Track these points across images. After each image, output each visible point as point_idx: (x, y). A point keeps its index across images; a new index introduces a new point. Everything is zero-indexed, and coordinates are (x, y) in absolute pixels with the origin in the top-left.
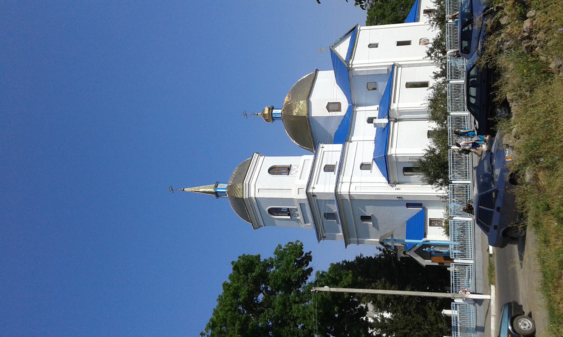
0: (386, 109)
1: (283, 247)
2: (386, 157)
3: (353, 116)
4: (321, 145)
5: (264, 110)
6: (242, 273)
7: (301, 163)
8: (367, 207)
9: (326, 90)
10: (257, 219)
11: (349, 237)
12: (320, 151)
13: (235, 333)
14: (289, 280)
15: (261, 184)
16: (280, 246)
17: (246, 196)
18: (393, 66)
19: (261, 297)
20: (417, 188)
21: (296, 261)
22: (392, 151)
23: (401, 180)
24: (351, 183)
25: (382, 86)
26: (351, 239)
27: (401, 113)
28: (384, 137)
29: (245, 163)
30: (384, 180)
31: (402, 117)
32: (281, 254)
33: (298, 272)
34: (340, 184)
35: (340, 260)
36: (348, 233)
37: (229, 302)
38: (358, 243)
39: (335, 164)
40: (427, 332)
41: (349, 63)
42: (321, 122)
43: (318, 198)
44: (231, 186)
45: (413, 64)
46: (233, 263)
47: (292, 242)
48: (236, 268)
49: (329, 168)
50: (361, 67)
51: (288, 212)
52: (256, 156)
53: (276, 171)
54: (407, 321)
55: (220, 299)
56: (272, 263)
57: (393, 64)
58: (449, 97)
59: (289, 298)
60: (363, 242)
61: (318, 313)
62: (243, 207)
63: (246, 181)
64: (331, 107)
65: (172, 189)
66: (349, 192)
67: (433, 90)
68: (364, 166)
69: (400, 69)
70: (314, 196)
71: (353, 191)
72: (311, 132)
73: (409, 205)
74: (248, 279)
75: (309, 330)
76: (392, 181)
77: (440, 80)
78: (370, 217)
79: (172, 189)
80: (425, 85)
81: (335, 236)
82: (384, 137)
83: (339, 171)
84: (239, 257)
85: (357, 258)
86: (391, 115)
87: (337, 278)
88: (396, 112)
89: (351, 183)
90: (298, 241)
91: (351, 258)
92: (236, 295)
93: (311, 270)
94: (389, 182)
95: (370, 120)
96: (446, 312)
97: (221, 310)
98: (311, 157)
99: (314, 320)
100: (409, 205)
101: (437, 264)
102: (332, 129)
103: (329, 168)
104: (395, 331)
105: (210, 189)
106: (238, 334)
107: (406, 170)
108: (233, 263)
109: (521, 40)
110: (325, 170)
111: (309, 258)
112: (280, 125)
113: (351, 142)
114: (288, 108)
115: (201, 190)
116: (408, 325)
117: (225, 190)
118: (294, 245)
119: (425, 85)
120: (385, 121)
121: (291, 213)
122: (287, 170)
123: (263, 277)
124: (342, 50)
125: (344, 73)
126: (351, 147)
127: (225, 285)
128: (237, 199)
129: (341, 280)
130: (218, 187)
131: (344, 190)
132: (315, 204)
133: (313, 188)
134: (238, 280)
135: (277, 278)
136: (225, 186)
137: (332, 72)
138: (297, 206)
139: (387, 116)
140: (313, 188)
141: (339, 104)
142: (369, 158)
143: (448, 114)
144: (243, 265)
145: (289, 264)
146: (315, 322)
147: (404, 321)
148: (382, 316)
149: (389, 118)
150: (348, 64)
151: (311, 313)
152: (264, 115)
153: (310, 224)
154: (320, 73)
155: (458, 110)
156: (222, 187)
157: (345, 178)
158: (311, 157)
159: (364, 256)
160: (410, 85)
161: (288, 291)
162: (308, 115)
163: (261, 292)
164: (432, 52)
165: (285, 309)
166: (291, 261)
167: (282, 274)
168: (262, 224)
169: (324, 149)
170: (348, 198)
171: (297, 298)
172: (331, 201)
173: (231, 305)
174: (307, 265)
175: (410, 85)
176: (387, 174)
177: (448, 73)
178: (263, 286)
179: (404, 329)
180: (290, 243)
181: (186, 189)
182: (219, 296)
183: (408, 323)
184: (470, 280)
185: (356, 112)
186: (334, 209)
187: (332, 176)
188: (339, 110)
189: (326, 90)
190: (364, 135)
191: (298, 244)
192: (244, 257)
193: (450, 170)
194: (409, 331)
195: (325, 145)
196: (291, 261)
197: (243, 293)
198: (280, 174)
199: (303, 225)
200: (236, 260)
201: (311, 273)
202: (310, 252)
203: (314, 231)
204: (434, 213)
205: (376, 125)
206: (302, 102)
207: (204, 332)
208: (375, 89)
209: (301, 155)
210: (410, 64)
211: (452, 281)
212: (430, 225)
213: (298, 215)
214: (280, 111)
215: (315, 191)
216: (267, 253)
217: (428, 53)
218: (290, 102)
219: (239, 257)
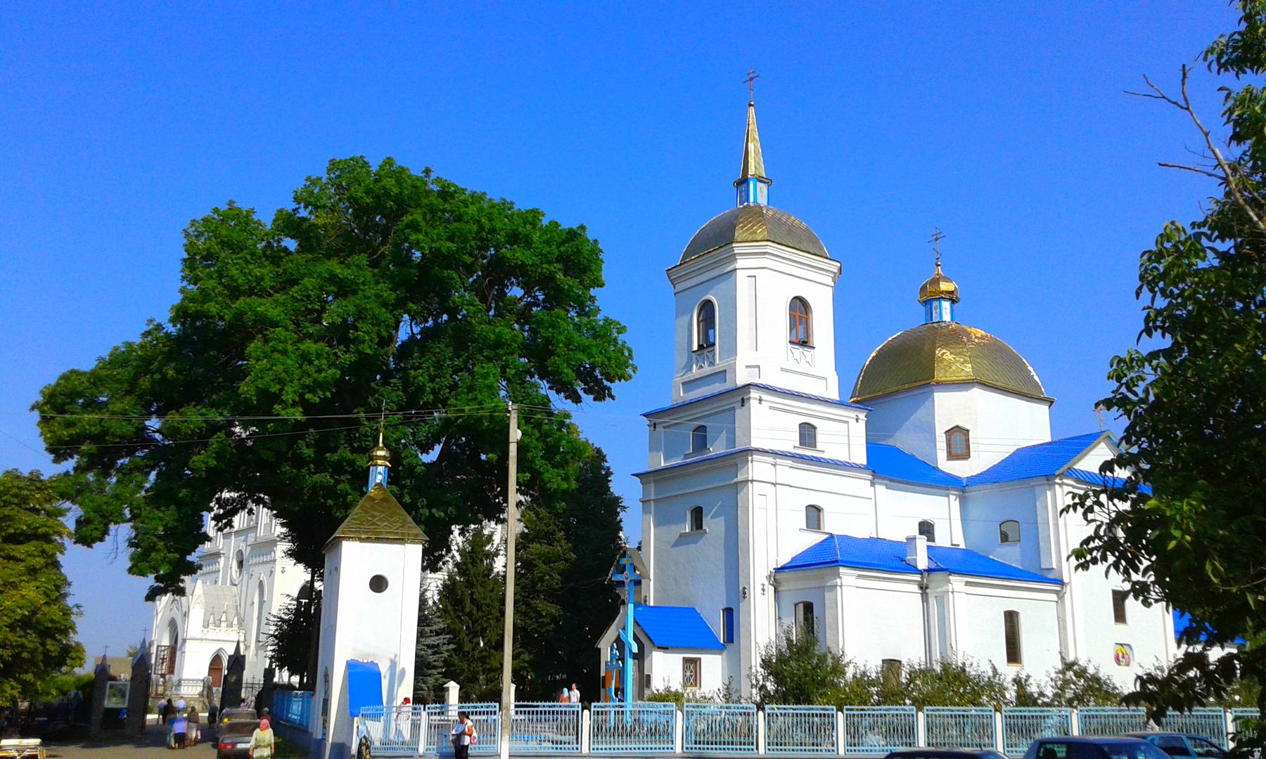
0: (948, 564)
1: (621, 338)
2: (835, 563)
3: (937, 488)
4: (862, 416)
5: (947, 280)
6: (562, 249)
7: (820, 370)
8: (721, 520)
9: (1001, 425)
10: (689, 276)
11: (655, 481)
12: (851, 414)
13: (433, 241)
14: (552, 353)
15: (766, 283)
16: (622, 330)
17: (738, 248)
18: (1061, 582)
19: (516, 292)
21: (593, 367)
22: (848, 577)
24: (775, 484)
25: (1009, 555)
26: (652, 486)
27: (941, 600)
28: (884, 559)
29: (815, 242)
30: (784, 560)
31: (932, 601)
32: (605, 334)
33: (569, 373)
34: (770, 459)
35: (610, 463)
36: (664, 479)
37: (498, 225)
38: (644, 502)
39: (819, 446)
40: (466, 649)
41: (1067, 477)
42: (920, 414)
43: (738, 411)
44: (762, 214)
45: (1065, 628)
46: (582, 228)
47: (634, 354)
48: (572, 235)
49: (807, 434)
51: (706, 345)
52: (834, 267)
53: (798, 314)
54: (488, 606)
55: (505, 206)
56: (587, 315)
57: (1066, 580)
58: (973, 711)
59: (512, 354)
60: (646, 511)
61: (481, 418)
62: (715, 244)
63: (772, 248)
64: (958, 437)
65: (751, 79)
66: (752, 481)
67: (990, 674)
68: (814, 515)
69: (1054, 597)
71: (754, 490)
72: (897, 392)
73: (729, 613)
74: (550, 263)
75: (448, 399)
76: (780, 576)
77: (1011, 694)
79: (751, 79)
80: (1013, 654)
81: (658, 450)
82: (884, 559)
83: (802, 458)
84: (596, 241)
85: (618, 498)
86: (936, 576)
87: (558, 457)
88: (945, 588)
89: (775, 484)
90: (635, 369)
91: (617, 486)
92: (515, 238)
93: (577, 399)
94: (778, 570)
95: (926, 529)
96: (453, 689)
97: (481, 210)
98: (834, 395)
99: (467, 408)
100: (729, 613)
101: (602, 674)
102: (905, 441)
103: (807, 434)
104: (468, 581)
105: (755, 166)
106: (431, 248)
107: (808, 608)
108: (582, 228)
111: (601, 393)
112: (914, 319)
113: (873, 484)
114: (954, 338)
115: (751, 146)
116: (479, 608)
117: (751, 199)
118: (626, 362)
119: (1013, 654)
120: (923, 563)
122: (803, 341)
123: (557, 298)
125: (1033, 468)
126: (861, 484)
127: (535, 214)
128: (732, 228)
129: (554, 466)
131: (758, 468)
132: (725, 404)
133: (760, 400)
134: (548, 243)
135: (553, 326)
136: (763, 201)
137: (1048, 439)
138: (719, 364)
139: (933, 566)
140: (760, 400)
141: (966, 456)
142: (834, 524)
143: (919, 709)
144: (578, 252)
145: (583, 351)
146: (463, 411)
147: (488, 601)
148: (496, 554)
149: (929, 571)
150: (1062, 476)
151: (480, 403)
152: (935, 281)
153: (682, 396)
154: (1043, 409)
155: (929, 729)
156: (759, 194)
157: (786, 472)
158: (834, 395)
159: (622, 515)
160: (1011, 619)
161: (528, 350)
162: (938, 383)
163: (528, 292)
164: (1076, 674)
165: (489, 347)
166: (590, 356)
167: (562, 338)
168: (679, 287)
170: (740, 478)
171: (513, 372)
172: (732, 440)
173: (493, 231)
174: (585, 391)
175: (1011, 619)
176: (797, 566)
177: (1027, 711)
178: (541, 297)
179: (473, 600)
180: (630, 351)
181: (752, 110)
182: (512, 203)
183: (484, 608)
184: (550, 745)
185: (947, 496)
187: (790, 442)
188: (951, 456)
189: (1001, 425)
190: (893, 514)
191: (629, 371)
192: (595, 251)
193: (791, 708)
194: (467, 610)
195: (862, 424)
196: (590, 356)
197: (518, 255)
198: (793, 326)
199: (679, 379)
200: (590, 235)
201: (569, 401)
202: (613, 397)
203: (667, 405)
204: (713, 668)
205: (911, 540)
206: (968, 368)
207: (433, 176)
208: (1004, 538)
209: (839, 368)
210: (1064, 621)
211: (543, 706)
212: (686, 660)
214: (947, 317)
215: (754, 404)
216: (608, 302)
217: (1074, 664)
218: (969, 340)
219: (596, 241)
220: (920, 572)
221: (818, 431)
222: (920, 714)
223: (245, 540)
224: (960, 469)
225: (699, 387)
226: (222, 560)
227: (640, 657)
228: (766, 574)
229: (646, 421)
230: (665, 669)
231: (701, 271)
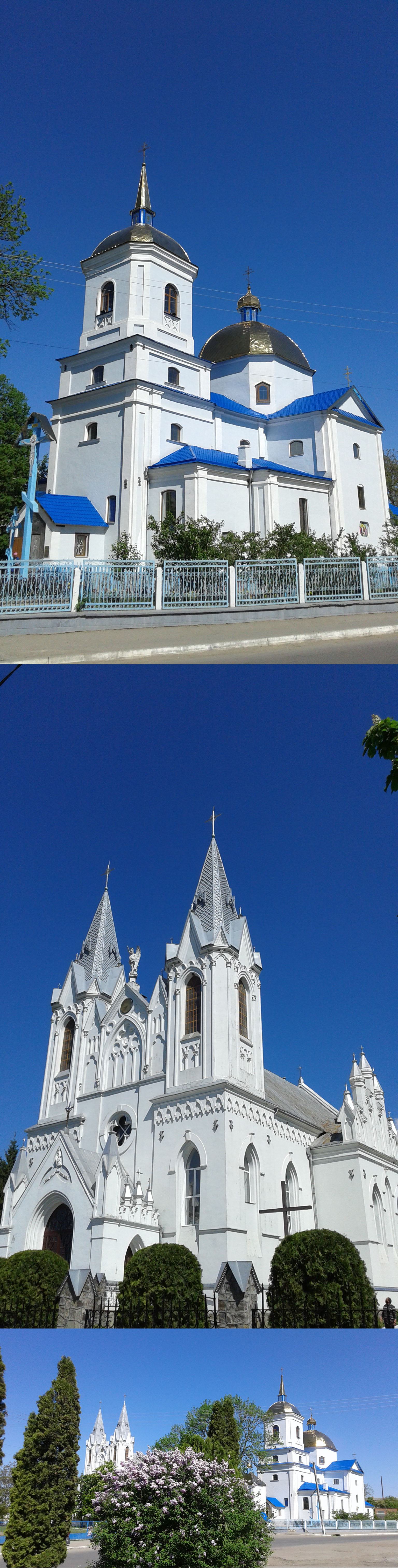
7: (182, 334)
18: (330, 481)
20: (140, 510)
28: (223, 464)
30: (156, 459)
39: (181, 385)
49: (173, 374)
50: (327, 438)
53: (170, 296)
57: (334, 479)
68: (176, 429)
70: (131, 348)
76: (154, 472)
82: (223, 464)
94: (151, 468)
103: (173, 374)
109: (361, 1293)
110: (171, 369)
122: (171, 310)
124: (350, 406)
126: (207, 414)
130: (147, 214)
137: (312, 394)
141: (268, 402)
142: (186, 437)
149: (254, 469)
154: (309, 379)
155: (309, 576)
157: (157, 399)
158: (191, 351)
160: (303, 501)
162: (252, 355)
169: (202, 371)
175: (303, 501)
176: (166, 463)
187: (162, 379)
188: (259, 402)
189: (289, 385)
190: (221, 437)
213: (102, 326)
220: (248, 470)
221: (180, 374)
222: (301, 565)
224: (266, 410)
227: (39, 531)
230: (60, 545)
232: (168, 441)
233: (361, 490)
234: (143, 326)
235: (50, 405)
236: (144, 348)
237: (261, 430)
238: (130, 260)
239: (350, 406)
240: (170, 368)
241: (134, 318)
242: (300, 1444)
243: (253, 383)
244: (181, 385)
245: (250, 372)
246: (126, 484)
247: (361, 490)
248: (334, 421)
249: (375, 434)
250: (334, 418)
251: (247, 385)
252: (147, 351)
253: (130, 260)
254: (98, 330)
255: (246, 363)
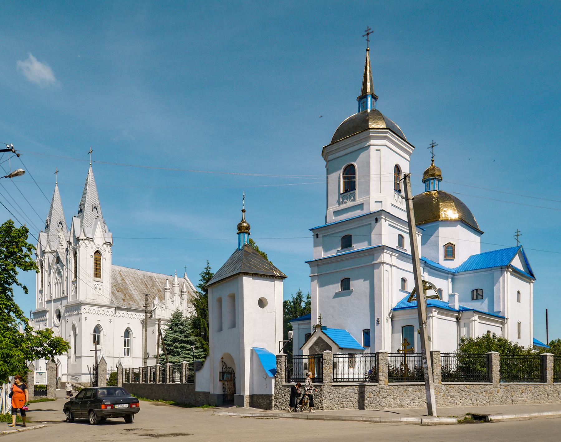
10: (338, 150)
18: (504, 318)
23: (395, 323)
30: (394, 305)
36: (349, 259)
50: (504, 287)
70: (377, 220)
73: (367, 333)
76: (397, 313)
78: (348, 288)
94: (395, 309)
121: (349, 193)
132: (365, 222)
137: (478, 252)
138: (358, 201)
157: (394, 260)
168: (330, 157)
186: (357, 247)
187: (394, 244)
195: (420, 237)
213: (346, 202)
221: (456, 248)
223: (61, 304)
225: (347, 212)
226: (48, 315)
228: (388, 313)
229: (312, 233)
231: (345, 147)
232: (400, 290)
233: (519, 324)
234: (381, 202)
235: (308, 265)
236: (385, 220)
237: (450, 280)
238: (370, 145)
239: (517, 263)
240: (399, 235)
241: (374, 195)
242: (397, 206)
243: (442, 244)
244: (405, 248)
245: (440, 235)
246: (378, 321)
247: (519, 324)
248: (509, 273)
249: (530, 283)
250: (510, 272)
251: (437, 245)
252: (387, 222)
253: (370, 145)
254: (343, 206)
255: (436, 229)
